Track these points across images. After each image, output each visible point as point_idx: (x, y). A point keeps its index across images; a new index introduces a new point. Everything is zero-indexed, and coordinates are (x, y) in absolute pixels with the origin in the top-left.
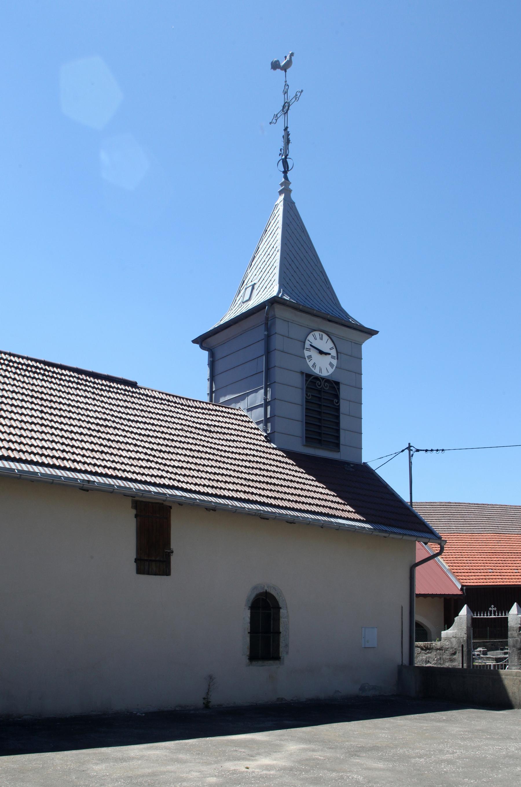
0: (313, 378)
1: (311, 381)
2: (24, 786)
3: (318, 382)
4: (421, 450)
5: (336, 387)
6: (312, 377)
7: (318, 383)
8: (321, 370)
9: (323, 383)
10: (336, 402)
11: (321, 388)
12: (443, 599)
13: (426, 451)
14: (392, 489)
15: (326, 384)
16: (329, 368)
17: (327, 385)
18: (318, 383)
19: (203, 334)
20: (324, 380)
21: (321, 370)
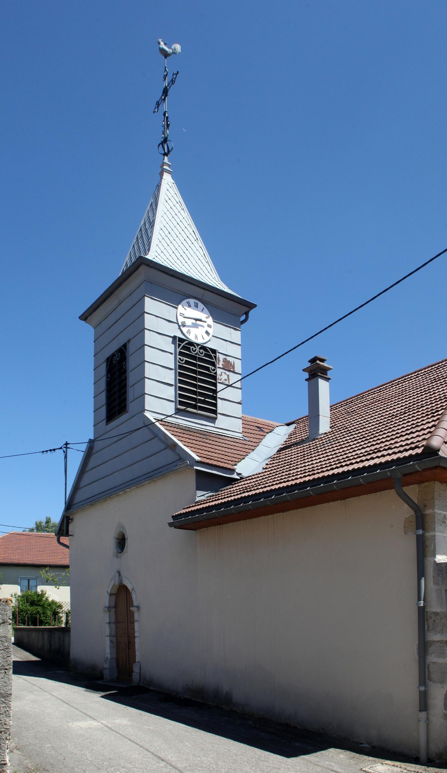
0: (186, 344)
1: (184, 346)
2: (2, 709)
3: (193, 347)
4: (56, 449)
5: (213, 355)
6: (186, 342)
7: (193, 349)
8: (196, 337)
9: (198, 349)
10: (213, 369)
11: (196, 354)
12: (70, 534)
13: (78, 450)
14: (80, 466)
15: (201, 351)
16: (205, 336)
17: (203, 352)
18: (193, 349)
19: (107, 290)
20: (199, 346)
21: (196, 337)
